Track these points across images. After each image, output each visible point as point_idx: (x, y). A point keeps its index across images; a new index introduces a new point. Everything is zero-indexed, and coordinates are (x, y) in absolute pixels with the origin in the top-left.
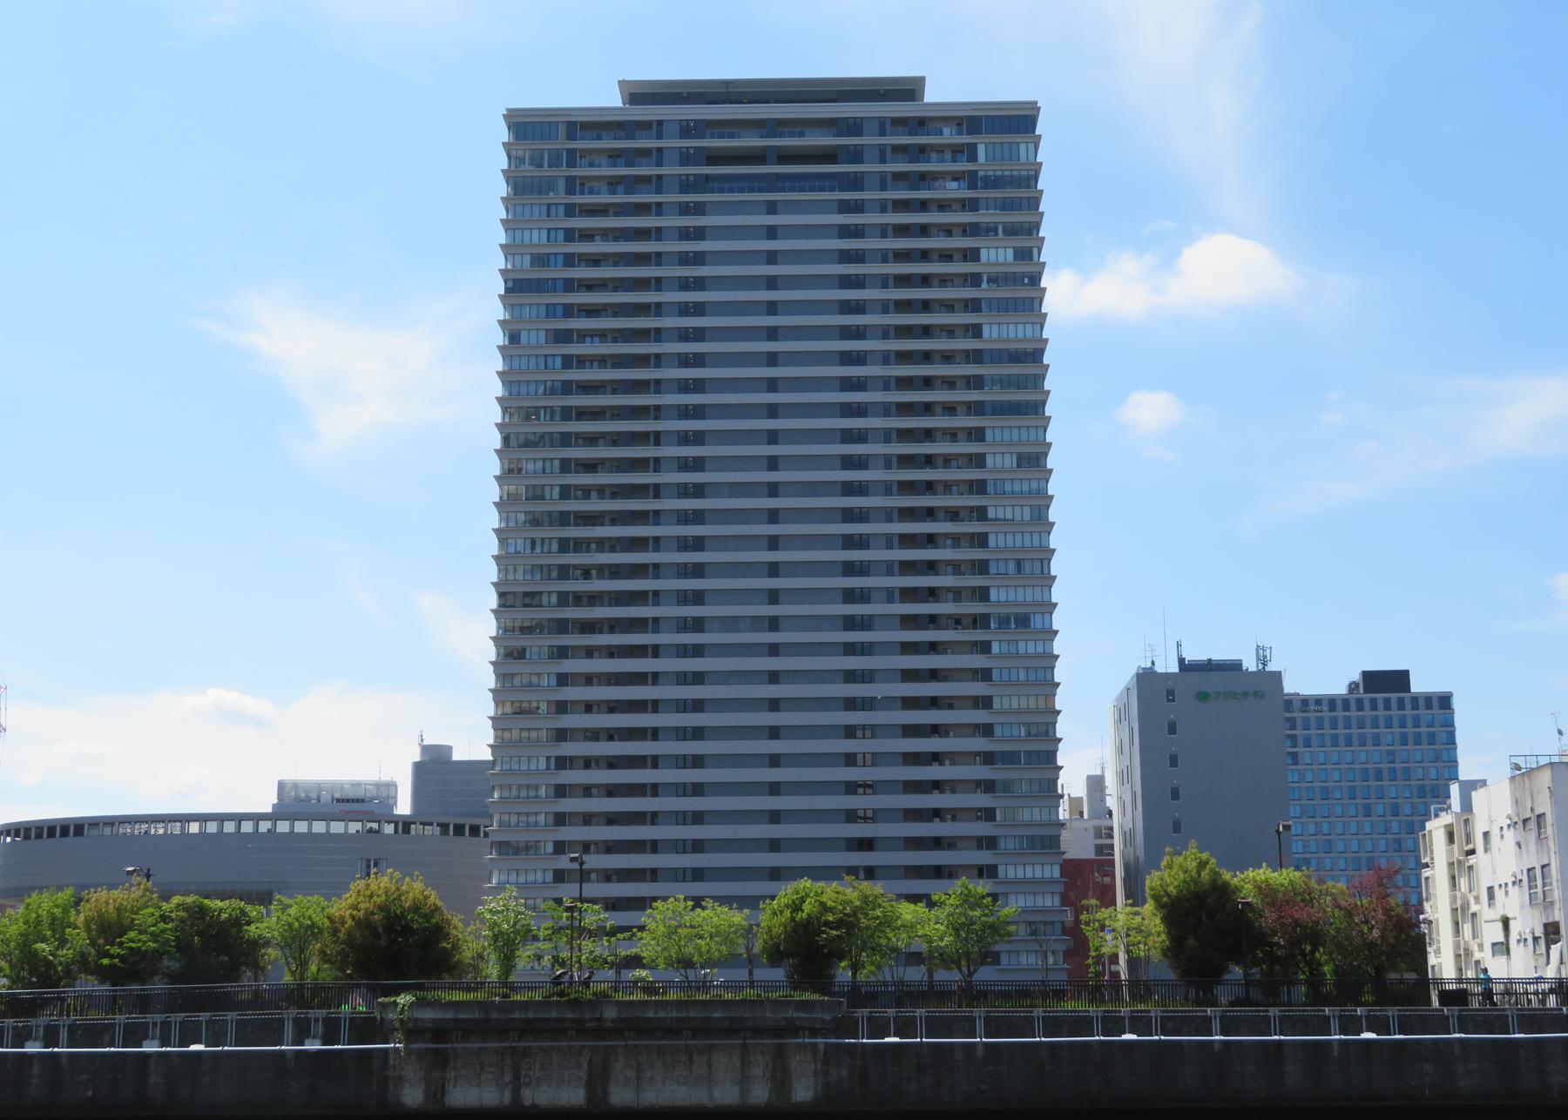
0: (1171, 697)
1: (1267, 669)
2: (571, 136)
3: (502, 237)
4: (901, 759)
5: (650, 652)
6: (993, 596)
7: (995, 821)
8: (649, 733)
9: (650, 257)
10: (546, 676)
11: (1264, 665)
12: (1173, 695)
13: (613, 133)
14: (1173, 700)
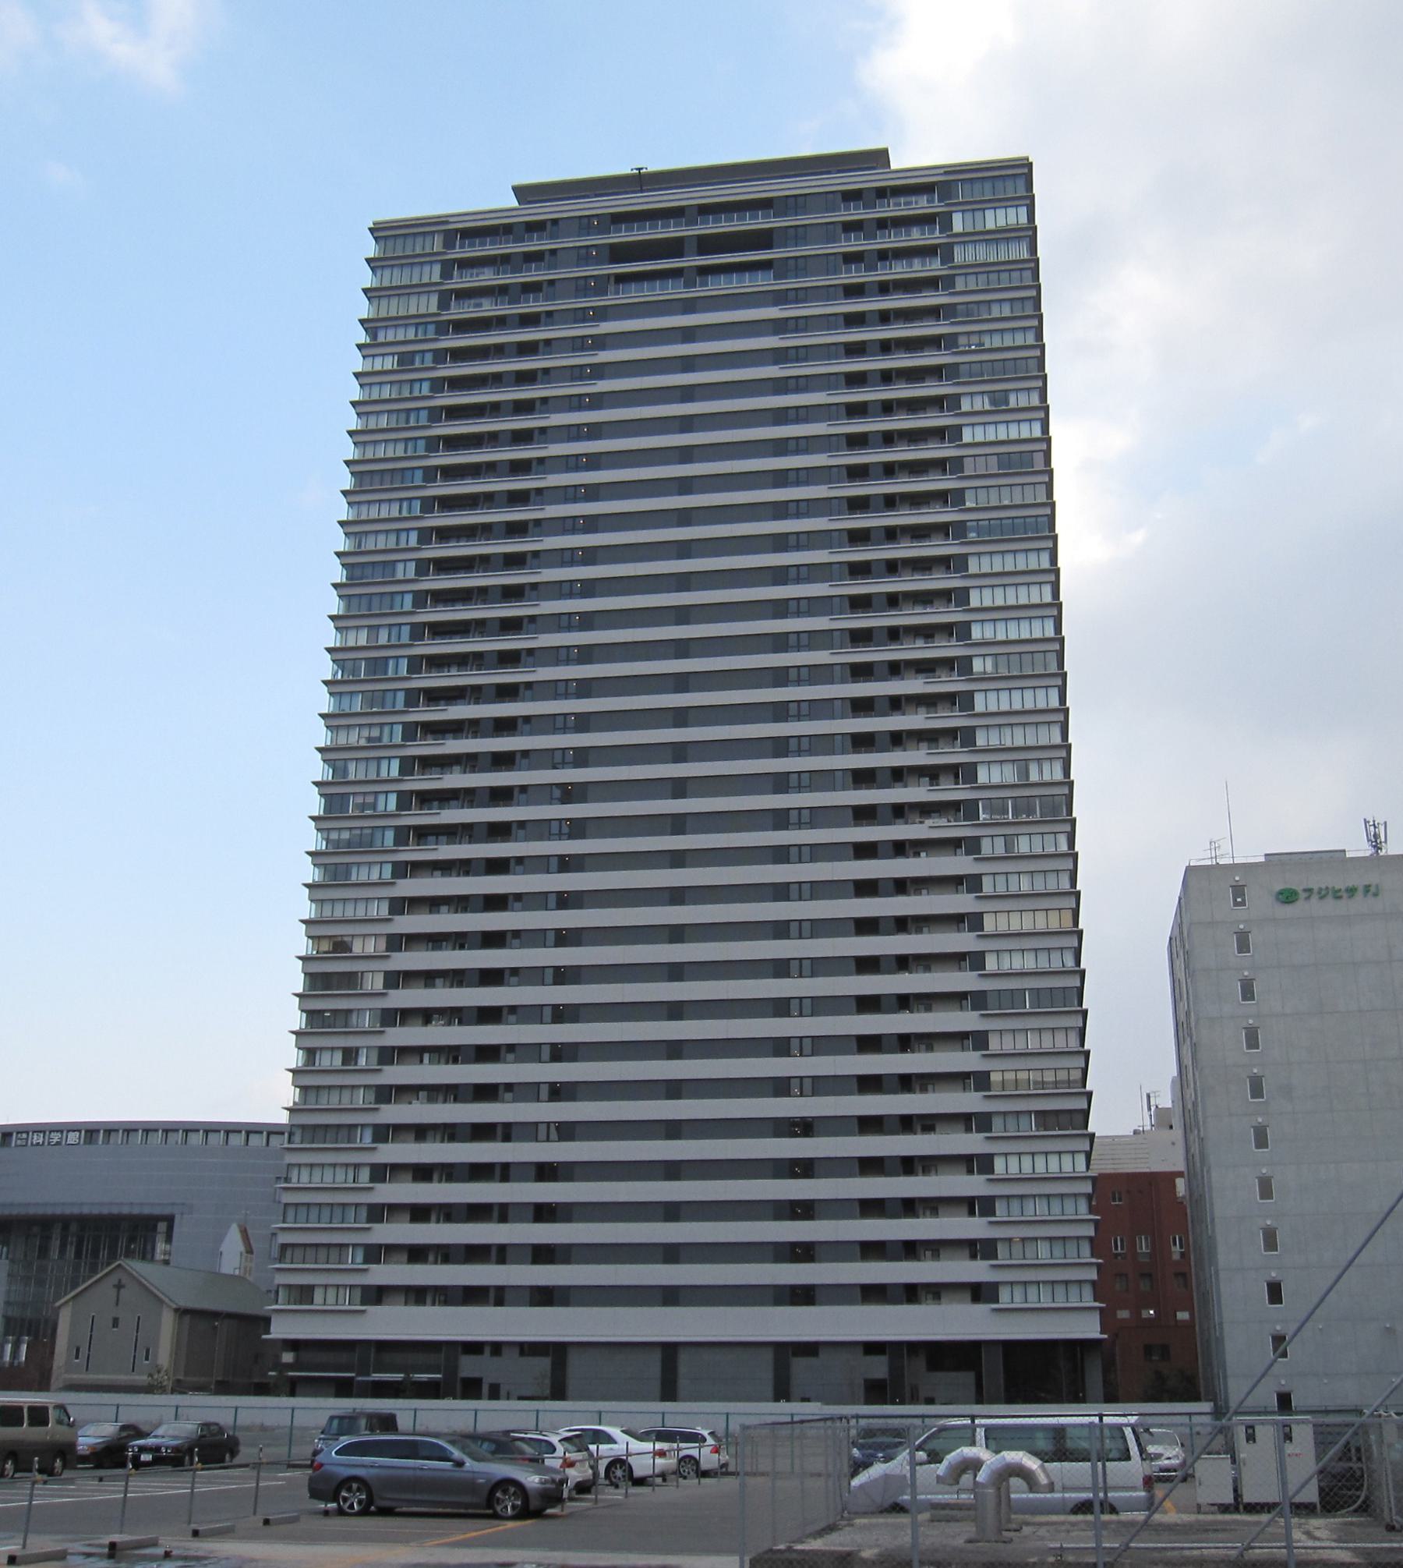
0: (1239, 900)
1: (1382, 853)
2: (449, 244)
3: (325, 702)
4: (853, 966)
5: (496, 1214)
6: (982, 777)
7: (992, 1172)
8: (492, 1294)
9: (489, 1252)
10: (365, 1050)
11: (1377, 847)
12: (1243, 895)
13: (494, 300)
14: (1243, 903)
